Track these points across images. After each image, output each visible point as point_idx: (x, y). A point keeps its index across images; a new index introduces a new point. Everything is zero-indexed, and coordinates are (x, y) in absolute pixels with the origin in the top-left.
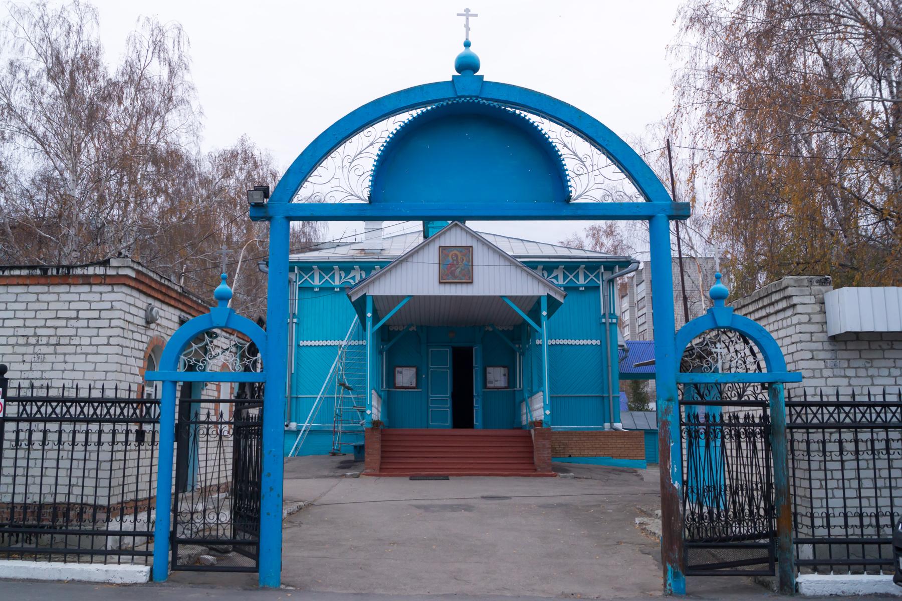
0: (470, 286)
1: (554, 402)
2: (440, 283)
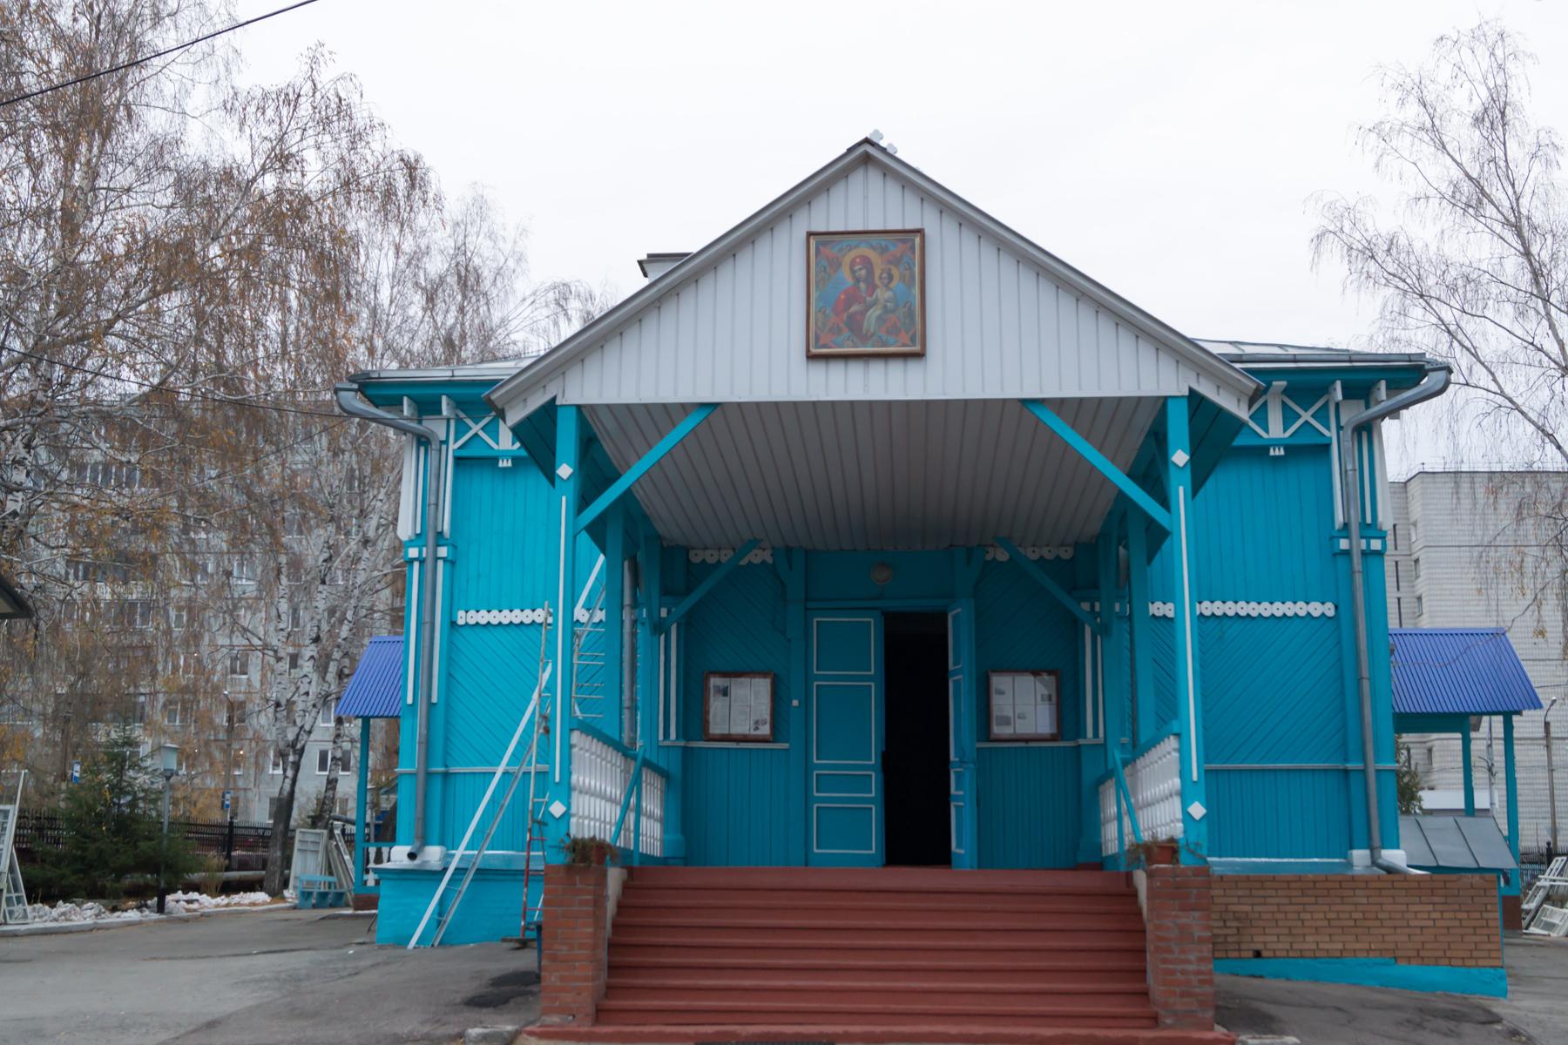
0: (913, 367)
1: (1218, 782)
2: (811, 357)
